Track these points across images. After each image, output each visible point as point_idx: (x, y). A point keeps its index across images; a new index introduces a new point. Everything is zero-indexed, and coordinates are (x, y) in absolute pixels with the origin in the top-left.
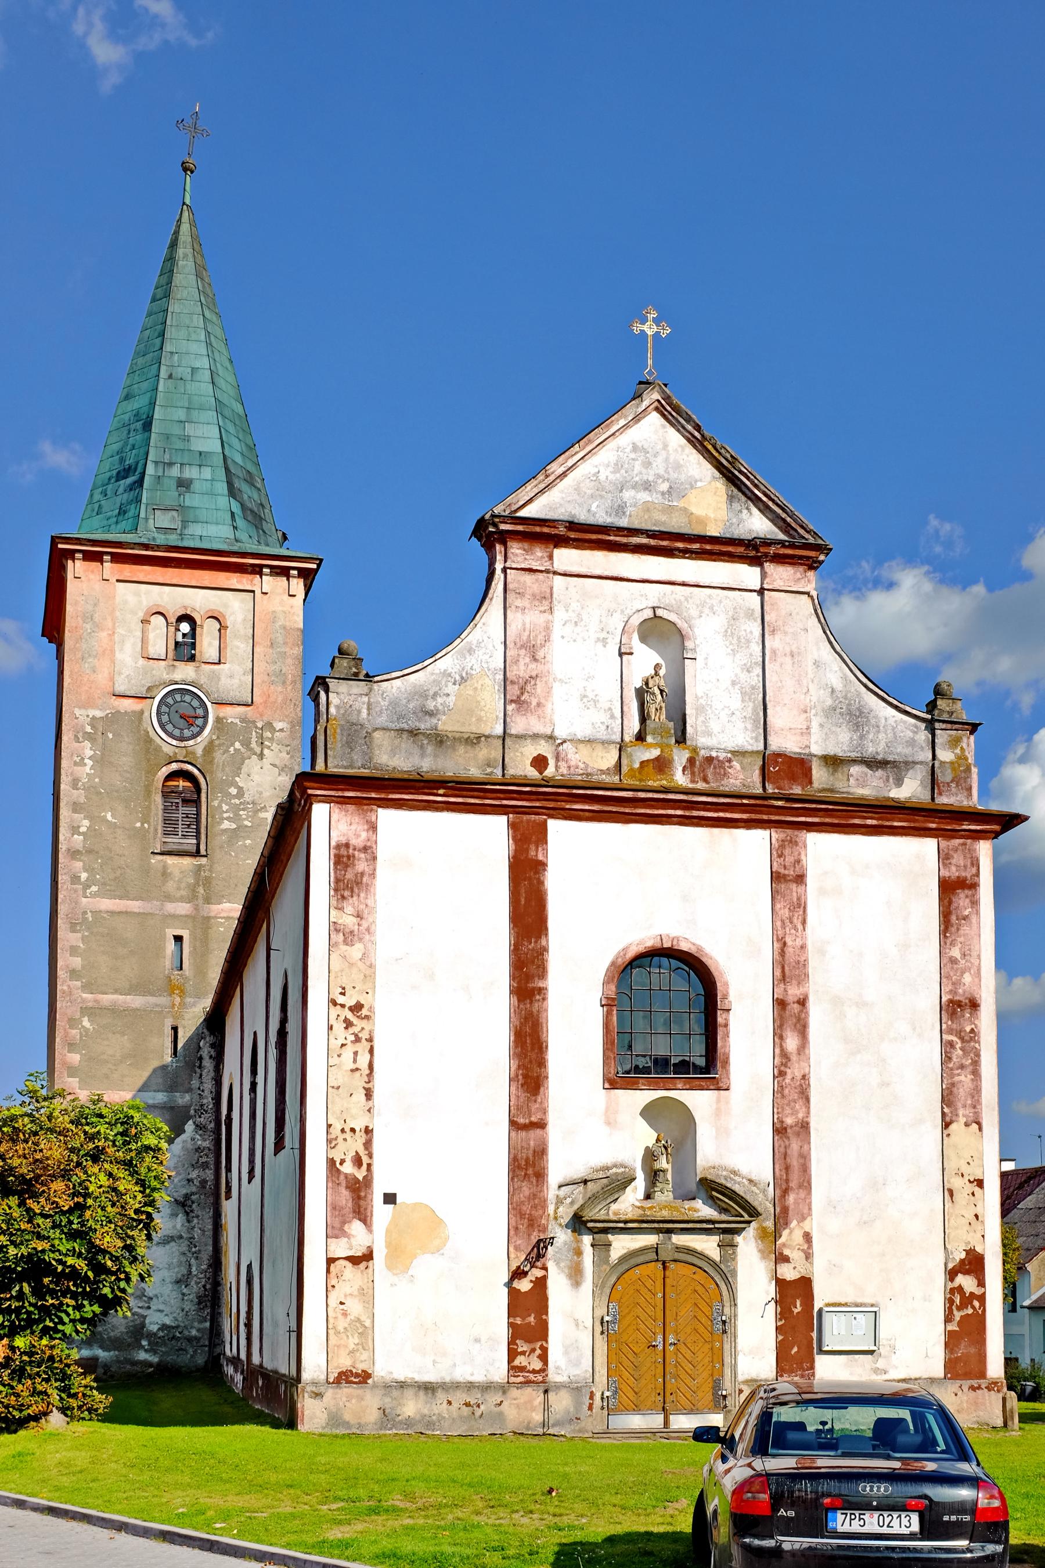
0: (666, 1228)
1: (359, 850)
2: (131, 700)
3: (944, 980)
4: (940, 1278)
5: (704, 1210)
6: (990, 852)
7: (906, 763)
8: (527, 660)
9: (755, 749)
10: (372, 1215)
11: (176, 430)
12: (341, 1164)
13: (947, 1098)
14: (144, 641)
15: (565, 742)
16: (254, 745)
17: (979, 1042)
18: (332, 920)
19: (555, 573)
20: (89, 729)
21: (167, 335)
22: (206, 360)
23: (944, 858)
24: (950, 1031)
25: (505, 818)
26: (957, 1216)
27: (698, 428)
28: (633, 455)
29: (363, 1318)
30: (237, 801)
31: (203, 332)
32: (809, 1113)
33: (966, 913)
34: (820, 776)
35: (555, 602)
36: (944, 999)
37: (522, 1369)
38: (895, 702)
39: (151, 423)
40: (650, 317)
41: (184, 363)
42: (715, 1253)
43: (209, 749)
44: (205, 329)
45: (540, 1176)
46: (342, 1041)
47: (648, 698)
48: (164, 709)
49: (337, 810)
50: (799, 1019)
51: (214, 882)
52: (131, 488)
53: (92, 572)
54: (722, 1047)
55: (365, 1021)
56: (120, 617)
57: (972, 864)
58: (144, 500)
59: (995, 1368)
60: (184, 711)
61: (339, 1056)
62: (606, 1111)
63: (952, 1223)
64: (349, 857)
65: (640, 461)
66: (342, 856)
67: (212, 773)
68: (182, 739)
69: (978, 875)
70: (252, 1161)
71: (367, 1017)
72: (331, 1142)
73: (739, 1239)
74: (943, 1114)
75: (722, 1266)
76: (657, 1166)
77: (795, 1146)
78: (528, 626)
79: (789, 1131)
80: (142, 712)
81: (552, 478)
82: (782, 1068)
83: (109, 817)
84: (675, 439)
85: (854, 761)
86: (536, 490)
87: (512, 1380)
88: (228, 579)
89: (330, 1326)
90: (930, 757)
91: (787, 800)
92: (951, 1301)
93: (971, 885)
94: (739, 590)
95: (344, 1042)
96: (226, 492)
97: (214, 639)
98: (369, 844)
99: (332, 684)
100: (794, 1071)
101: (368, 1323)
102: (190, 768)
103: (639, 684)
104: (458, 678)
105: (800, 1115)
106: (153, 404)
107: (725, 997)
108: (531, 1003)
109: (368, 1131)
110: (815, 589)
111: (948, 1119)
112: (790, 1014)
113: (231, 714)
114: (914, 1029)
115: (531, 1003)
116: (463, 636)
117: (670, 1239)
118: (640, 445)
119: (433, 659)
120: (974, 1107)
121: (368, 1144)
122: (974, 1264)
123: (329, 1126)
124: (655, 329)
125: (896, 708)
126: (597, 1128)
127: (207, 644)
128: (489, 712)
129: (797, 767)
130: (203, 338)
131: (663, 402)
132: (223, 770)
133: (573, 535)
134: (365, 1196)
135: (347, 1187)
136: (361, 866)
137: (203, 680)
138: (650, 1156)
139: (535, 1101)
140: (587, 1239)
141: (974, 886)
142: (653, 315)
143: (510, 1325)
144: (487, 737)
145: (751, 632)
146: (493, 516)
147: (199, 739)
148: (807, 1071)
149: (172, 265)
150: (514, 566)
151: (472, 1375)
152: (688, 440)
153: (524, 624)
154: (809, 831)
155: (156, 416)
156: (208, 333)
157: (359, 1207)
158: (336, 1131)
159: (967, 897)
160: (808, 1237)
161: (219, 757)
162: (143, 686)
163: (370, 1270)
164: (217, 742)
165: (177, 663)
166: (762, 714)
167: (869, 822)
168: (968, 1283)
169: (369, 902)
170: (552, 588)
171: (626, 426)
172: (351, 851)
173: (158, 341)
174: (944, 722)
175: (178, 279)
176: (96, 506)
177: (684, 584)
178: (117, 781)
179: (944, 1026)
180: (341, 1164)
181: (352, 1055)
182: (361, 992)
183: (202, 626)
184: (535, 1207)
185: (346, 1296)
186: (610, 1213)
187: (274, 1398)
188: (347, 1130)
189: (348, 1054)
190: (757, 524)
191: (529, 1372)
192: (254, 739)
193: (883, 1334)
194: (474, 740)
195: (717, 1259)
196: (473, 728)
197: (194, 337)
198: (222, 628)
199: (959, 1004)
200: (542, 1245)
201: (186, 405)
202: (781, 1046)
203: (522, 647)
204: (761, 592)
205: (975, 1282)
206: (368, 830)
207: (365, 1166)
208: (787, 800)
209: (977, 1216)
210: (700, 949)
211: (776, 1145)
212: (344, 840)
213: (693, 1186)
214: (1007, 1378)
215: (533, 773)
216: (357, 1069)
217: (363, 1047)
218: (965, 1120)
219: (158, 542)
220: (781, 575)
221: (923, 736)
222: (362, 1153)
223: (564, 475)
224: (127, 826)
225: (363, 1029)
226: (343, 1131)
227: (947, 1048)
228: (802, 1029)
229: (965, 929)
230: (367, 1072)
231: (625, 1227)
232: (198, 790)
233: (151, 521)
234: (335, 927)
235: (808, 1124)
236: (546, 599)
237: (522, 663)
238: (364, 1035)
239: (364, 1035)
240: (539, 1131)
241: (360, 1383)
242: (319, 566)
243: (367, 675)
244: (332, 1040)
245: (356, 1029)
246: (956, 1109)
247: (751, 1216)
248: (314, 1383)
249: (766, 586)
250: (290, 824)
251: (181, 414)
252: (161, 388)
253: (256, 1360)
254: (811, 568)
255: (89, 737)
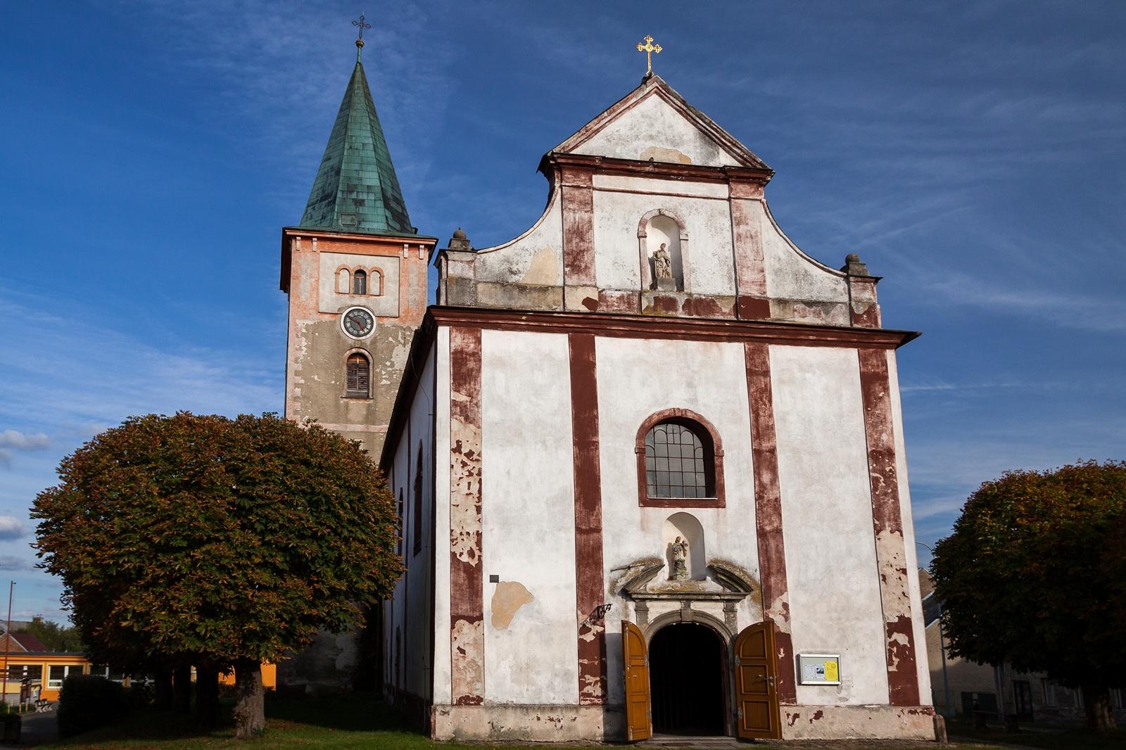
0: (687, 597)
1: (470, 355)
2: (329, 315)
3: (868, 438)
4: (881, 635)
5: (711, 585)
6: (894, 357)
7: (831, 303)
8: (578, 240)
9: (730, 294)
10: (482, 590)
11: (355, 175)
12: (460, 556)
13: (877, 514)
14: (337, 284)
15: (604, 290)
16: (400, 338)
17: (896, 478)
18: (452, 398)
19: (594, 189)
20: (304, 331)
21: (349, 127)
22: (370, 139)
23: (863, 360)
24: (874, 470)
25: (567, 335)
26: (889, 593)
27: (684, 102)
28: (642, 120)
29: (477, 660)
30: (391, 369)
31: (369, 126)
32: (781, 523)
33: (881, 395)
34: (775, 312)
35: (594, 207)
36: (869, 450)
37: (589, 695)
38: (822, 266)
39: (339, 172)
40: (649, 41)
41: (358, 141)
42: (721, 616)
43: (374, 341)
44: (371, 124)
45: (598, 564)
46: (459, 475)
47: (657, 264)
48: (348, 320)
49: (454, 330)
50: (770, 462)
51: (377, 414)
52: (329, 204)
53: (306, 247)
54: (719, 480)
55: (475, 462)
56: (323, 274)
57: (883, 365)
58: (336, 210)
59: (926, 697)
60: (358, 321)
61: (458, 485)
62: (642, 522)
63: (886, 598)
64: (462, 359)
65: (649, 124)
66: (459, 358)
67: (375, 354)
68: (358, 335)
69: (887, 370)
70: (398, 654)
71: (477, 460)
72: (453, 542)
73: (738, 606)
74: (875, 525)
75: (727, 625)
76: (677, 558)
77: (772, 544)
78: (577, 220)
79: (768, 535)
80: (335, 322)
81: (589, 133)
82: (761, 494)
83: (316, 378)
84: (668, 110)
85: (797, 302)
86: (580, 140)
87: (582, 703)
88: (384, 251)
89: (454, 666)
90: (848, 299)
91: (753, 324)
92: (890, 652)
93: (884, 378)
94: (715, 199)
95: (462, 476)
96: (383, 206)
97: (377, 283)
98: (476, 351)
99: (451, 255)
100: (771, 495)
101: (480, 663)
102: (363, 351)
103: (650, 255)
104: (532, 252)
105: (775, 525)
106: (341, 162)
107: (720, 447)
108: (588, 451)
109: (479, 534)
110: (764, 198)
111: (878, 528)
112: (764, 459)
113: (387, 323)
114: (850, 469)
115: (588, 451)
116: (535, 226)
117: (689, 606)
118: (646, 114)
119: (516, 240)
120: (896, 521)
121: (479, 543)
122: (904, 625)
123: (452, 531)
124: (652, 48)
125: (822, 268)
126: (635, 532)
127: (373, 285)
128: (554, 272)
129: (761, 305)
130: (369, 128)
131: (660, 88)
132: (382, 352)
133: (604, 166)
134: (477, 577)
135: (464, 572)
136: (471, 364)
137: (370, 305)
138: (672, 551)
139: (593, 515)
140: (632, 605)
141: (885, 378)
142: (651, 40)
143: (580, 664)
144: (552, 287)
145: (724, 224)
146: (553, 153)
147: (368, 336)
148: (778, 496)
149: (351, 93)
150: (567, 184)
151: (554, 699)
152: (677, 110)
153: (575, 219)
154: (771, 343)
155: (343, 168)
156: (372, 127)
157: (473, 584)
158: (456, 534)
159: (880, 385)
160: (785, 606)
161: (379, 345)
162: (336, 308)
163: (481, 627)
164: (379, 337)
165: (355, 296)
166: (733, 273)
167: (811, 337)
168: (902, 639)
169: (477, 387)
170: (592, 198)
171: (637, 103)
172: (464, 356)
173: (343, 131)
174: (856, 276)
175: (355, 99)
176: (309, 216)
177: (678, 195)
178: (321, 359)
179: (871, 467)
180: (460, 556)
181: (467, 484)
182: (472, 444)
183: (369, 276)
184: (594, 584)
185: (464, 644)
186: (648, 590)
187: (415, 711)
188: (464, 533)
189: (464, 484)
190: (724, 159)
191: (594, 697)
192: (400, 336)
193: (843, 674)
194: (544, 289)
195: (723, 620)
196: (543, 282)
197: (364, 128)
198: (382, 277)
199: (880, 453)
200: (601, 610)
201: (360, 162)
202: (759, 480)
203: (574, 233)
204: (729, 199)
205: (907, 638)
206: (475, 343)
207: (477, 557)
208: (753, 324)
209: (904, 593)
210: (701, 417)
211: (760, 544)
212: (459, 349)
213: (703, 572)
214: (934, 706)
215: (584, 309)
216: (470, 494)
217: (475, 478)
218: (890, 529)
219: (344, 231)
220: (742, 189)
221: (842, 285)
222: (475, 548)
223: (598, 131)
224: (326, 383)
225: (474, 467)
226: (461, 534)
227: (875, 482)
228: (773, 469)
229: (881, 405)
230: (478, 495)
231: (659, 597)
232: (369, 364)
233: (340, 221)
234: (454, 403)
235: (781, 530)
236: (588, 205)
237: (574, 242)
238: (475, 472)
239: (475, 472)
240: (596, 535)
241: (475, 704)
242: (436, 243)
243: (473, 249)
244: (453, 475)
245: (470, 468)
246: (884, 522)
247: (746, 591)
248: (443, 705)
249: (732, 196)
250: (423, 344)
251: (356, 167)
252: (345, 153)
253: (402, 687)
254: (761, 185)
255: (303, 335)
